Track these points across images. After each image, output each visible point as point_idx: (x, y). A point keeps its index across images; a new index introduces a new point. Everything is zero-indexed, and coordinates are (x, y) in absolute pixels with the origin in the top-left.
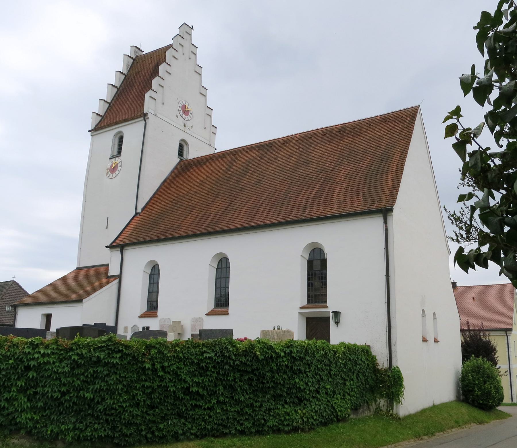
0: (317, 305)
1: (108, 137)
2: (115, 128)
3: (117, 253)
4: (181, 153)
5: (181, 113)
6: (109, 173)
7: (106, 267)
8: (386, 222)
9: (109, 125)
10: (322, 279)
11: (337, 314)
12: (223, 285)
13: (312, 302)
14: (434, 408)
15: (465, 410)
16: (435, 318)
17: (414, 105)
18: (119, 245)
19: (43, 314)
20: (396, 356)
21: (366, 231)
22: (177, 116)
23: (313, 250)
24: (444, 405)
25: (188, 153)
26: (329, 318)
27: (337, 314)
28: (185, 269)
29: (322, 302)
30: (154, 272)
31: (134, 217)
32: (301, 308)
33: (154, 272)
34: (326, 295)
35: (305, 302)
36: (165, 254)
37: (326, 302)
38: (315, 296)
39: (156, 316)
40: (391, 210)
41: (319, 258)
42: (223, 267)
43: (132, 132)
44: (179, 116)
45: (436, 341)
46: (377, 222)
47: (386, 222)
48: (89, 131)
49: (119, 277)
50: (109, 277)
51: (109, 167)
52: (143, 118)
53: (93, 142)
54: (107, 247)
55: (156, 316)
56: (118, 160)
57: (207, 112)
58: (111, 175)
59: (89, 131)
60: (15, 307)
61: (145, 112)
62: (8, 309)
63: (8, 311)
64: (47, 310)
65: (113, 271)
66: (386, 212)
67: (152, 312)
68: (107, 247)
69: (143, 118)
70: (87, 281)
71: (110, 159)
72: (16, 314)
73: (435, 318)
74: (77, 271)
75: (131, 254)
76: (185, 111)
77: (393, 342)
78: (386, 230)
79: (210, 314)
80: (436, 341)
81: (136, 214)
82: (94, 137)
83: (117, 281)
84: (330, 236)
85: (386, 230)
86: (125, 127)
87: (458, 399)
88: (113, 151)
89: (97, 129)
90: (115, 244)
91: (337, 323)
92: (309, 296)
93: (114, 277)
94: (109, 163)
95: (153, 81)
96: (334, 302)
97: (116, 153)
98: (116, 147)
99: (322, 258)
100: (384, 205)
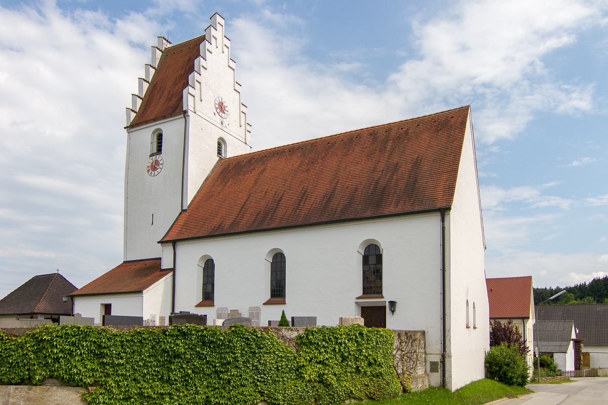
0: (372, 295)
1: (146, 135)
2: (154, 125)
3: (169, 249)
4: (219, 153)
5: (218, 111)
6: (151, 171)
7: (157, 261)
8: (443, 220)
9: (147, 122)
10: (377, 272)
11: (393, 304)
12: (210, 274)
13: (368, 293)
14: (473, 384)
15: (495, 384)
16: (474, 308)
17: (464, 105)
18: (172, 241)
19: (101, 304)
20: (450, 340)
21: (424, 228)
22: (214, 113)
23: (369, 246)
24: (479, 381)
25: (226, 151)
26: (385, 307)
27: (393, 304)
28: (241, 264)
29: (377, 293)
30: (209, 267)
31: (181, 213)
32: (357, 298)
33: (209, 267)
34: (381, 287)
35: (360, 293)
36: (224, 252)
37: (381, 293)
38: (371, 287)
39: (212, 305)
40: (449, 209)
41: (374, 254)
42: (278, 262)
43: (170, 128)
44: (216, 113)
45: (475, 328)
46: (435, 220)
47: (443, 220)
48: (125, 128)
49: (173, 270)
50: (162, 270)
51: (150, 164)
52: (182, 116)
53: (129, 139)
54: (158, 242)
55: (212, 305)
56: (159, 158)
57: (241, 110)
58: (153, 172)
59: (125, 128)
60: (72, 298)
61: (184, 110)
62: (64, 299)
63: (65, 301)
64: (106, 300)
65: (166, 264)
66: (444, 211)
67: (207, 302)
68: (158, 242)
69: (182, 116)
70: (140, 273)
71: (150, 156)
72: (73, 304)
73: (474, 308)
74: (125, 264)
75: (182, 249)
76: (221, 107)
77: (447, 328)
78: (443, 228)
79: (267, 303)
80: (475, 328)
81: (183, 211)
82: (130, 133)
83: (171, 274)
84: (383, 233)
85: (443, 228)
86: (162, 125)
87: (486, 376)
88: (152, 149)
89: (132, 126)
90: (166, 239)
91: (393, 312)
92: (364, 288)
93: (167, 271)
94: (149, 161)
95: (189, 76)
96: (388, 295)
97: (155, 151)
98: (155, 144)
99: (377, 253)
100: (440, 205)
